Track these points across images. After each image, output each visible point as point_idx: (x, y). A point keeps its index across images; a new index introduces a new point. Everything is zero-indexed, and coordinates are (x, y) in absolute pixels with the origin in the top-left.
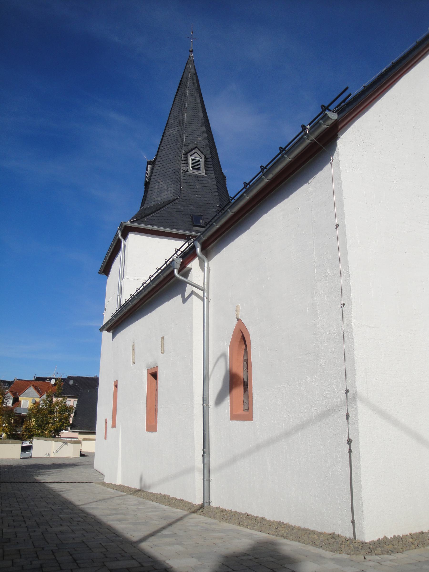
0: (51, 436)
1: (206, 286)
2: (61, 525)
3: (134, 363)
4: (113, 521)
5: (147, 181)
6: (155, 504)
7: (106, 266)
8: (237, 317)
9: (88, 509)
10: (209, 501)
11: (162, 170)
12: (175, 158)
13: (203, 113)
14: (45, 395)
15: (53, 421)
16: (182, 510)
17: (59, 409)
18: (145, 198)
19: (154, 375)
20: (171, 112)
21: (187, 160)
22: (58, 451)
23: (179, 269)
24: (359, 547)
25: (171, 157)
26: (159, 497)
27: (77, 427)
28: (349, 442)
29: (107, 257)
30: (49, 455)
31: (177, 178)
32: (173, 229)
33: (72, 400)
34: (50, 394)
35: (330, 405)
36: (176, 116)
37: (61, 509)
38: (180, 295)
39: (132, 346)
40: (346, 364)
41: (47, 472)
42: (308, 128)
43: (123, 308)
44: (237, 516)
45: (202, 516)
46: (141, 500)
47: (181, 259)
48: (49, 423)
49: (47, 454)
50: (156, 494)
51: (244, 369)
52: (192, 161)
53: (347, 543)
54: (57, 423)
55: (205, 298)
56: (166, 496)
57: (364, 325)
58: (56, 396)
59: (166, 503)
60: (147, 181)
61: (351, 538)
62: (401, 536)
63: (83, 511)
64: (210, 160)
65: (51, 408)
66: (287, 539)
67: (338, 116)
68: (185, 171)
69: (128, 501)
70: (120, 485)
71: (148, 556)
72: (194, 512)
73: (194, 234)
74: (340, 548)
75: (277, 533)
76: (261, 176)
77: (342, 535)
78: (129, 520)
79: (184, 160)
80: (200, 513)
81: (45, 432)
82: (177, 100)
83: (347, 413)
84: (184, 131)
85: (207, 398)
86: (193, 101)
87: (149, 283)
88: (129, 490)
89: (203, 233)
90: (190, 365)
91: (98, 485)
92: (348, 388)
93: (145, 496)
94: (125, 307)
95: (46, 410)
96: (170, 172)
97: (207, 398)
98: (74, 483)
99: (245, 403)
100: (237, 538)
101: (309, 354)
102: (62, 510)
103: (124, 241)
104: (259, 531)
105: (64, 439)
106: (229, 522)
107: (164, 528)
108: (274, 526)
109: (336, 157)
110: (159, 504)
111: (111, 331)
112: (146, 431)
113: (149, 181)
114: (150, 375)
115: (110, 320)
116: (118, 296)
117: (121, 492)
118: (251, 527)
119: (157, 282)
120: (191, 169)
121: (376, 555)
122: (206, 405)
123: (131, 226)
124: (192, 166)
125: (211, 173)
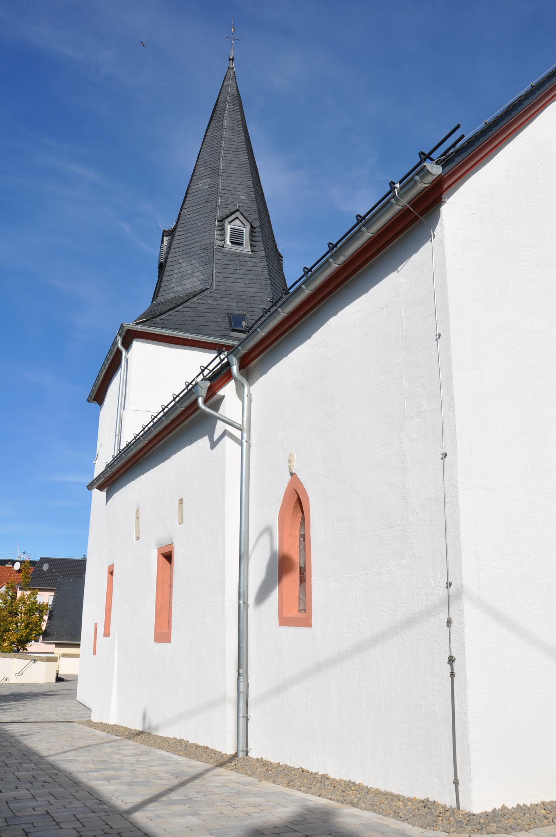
0: (12, 651)
1: (245, 423)
2: (17, 788)
3: (138, 538)
4: (97, 780)
5: (163, 261)
6: (165, 753)
7: (99, 389)
8: (291, 470)
9: (59, 763)
10: (247, 749)
11: (184, 244)
12: (205, 226)
13: (248, 156)
14: (4, 586)
15: (15, 626)
16: (205, 762)
17: (25, 608)
18: (158, 287)
19: (168, 557)
20: (199, 155)
21: (223, 229)
22: (22, 674)
23: (205, 397)
24: (463, 821)
25: (199, 224)
26: (172, 744)
27: (53, 635)
28: (451, 660)
29: (100, 377)
30: (8, 680)
31: (208, 257)
32: (201, 334)
33: (47, 594)
34: (11, 585)
35: (423, 604)
36: (207, 161)
37: (20, 764)
38: (206, 436)
39: (135, 512)
40: (448, 543)
41: (3, 706)
42: (397, 188)
43: (122, 455)
44: (286, 772)
45: (233, 772)
46: (144, 747)
47: (209, 382)
48: (9, 630)
49: (5, 678)
50: (169, 738)
51: (301, 549)
52: (231, 231)
53: (446, 815)
54: (22, 630)
55: (244, 441)
56: (183, 741)
57: (476, 485)
58: (21, 589)
59: (182, 752)
60: (162, 262)
61: (453, 807)
62: (529, 806)
63: (52, 766)
64: (258, 230)
65: (13, 606)
66: (357, 807)
67: (443, 169)
68: (221, 247)
69: (124, 749)
70: (114, 725)
71: (145, 833)
72: (221, 765)
73: (232, 342)
74: (436, 822)
75: (344, 799)
76: (328, 260)
77: (440, 802)
78: (122, 778)
79: (219, 230)
80: (232, 768)
81: (3, 644)
82: (209, 137)
83: (448, 617)
84: (219, 185)
85: (246, 592)
86: (235, 138)
87: (161, 418)
88: (128, 733)
89: (243, 342)
90: (220, 542)
91: (81, 726)
92: (450, 580)
93: (152, 741)
94: (125, 453)
95: (6, 610)
96: (197, 248)
97: (246, 592)
98: (44, 722)
99: (301, 600)
100: (282, 805)
101: (395, 528)
102: (21, 764)
103: (125, 354)
104: (316, 796)
105: (32, 655)
106: (273, 781)
107: (172, 790)
108: (340, 787)
109: (440, 232)
110: (172, 754)
111: (104, 489)
112: (155, 642)
113: (165, 261)
114: (161, 556)
115: (104, 473)
116: (116, 437)
117: (115, 736)
118: (306, 789)
119: (173, 417)
120: (229, 243)
121: (488, 833)
122: (243, 603)
123: (136, 330)
124: (231, 239)
125: (260, 250)
